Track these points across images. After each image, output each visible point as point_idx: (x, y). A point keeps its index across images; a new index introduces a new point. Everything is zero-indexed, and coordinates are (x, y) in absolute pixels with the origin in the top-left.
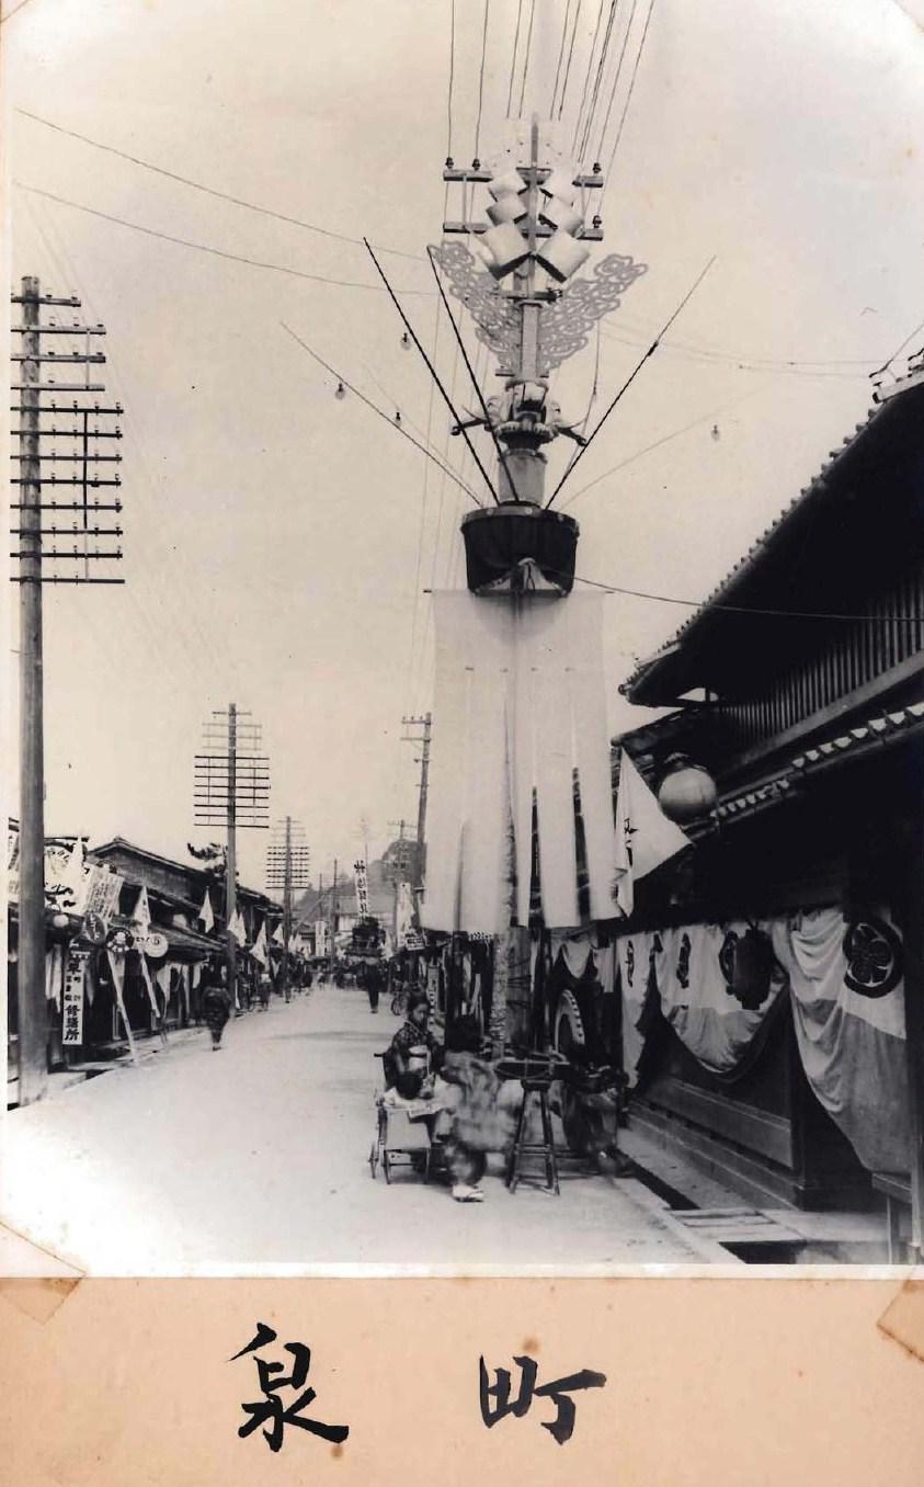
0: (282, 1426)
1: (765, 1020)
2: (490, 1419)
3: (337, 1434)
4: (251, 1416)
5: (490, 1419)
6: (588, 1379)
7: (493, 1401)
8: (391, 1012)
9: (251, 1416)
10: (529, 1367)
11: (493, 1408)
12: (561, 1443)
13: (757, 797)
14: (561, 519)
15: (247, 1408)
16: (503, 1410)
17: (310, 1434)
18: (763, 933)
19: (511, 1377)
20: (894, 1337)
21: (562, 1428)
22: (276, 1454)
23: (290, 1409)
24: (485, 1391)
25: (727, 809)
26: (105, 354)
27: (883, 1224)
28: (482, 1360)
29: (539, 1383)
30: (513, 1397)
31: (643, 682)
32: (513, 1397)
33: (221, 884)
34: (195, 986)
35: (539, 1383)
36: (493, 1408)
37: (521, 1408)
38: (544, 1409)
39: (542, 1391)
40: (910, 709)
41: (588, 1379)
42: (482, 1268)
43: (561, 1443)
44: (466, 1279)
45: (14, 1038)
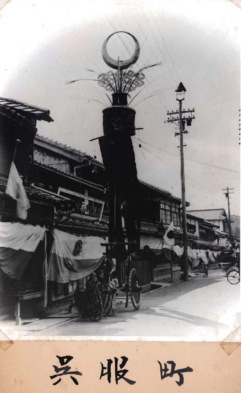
0: (103, 370)
1: (129, 274)
2: (163, 377)
3: (132, 382)
5: (163, 377)
6: (189, 369)
7: (163, 372)
11: (163, 374)
12: (114, 358)
13: (78, 248)
14: (44, 226)
16: (166, 376)
17: (126, 382)
22: (193, 372)
23: (120, 375)
24: (162, 370)
26: (176, 100)
29: (176, 369)
32: (169, 372)
33: (205, 246)
34: (88, 279)
35: (176, 369)
36: (163, 374)
37: (171, 375)
38: (176, 377)
40: (123, 227)
41: (189, 369)
43: (114, 358)
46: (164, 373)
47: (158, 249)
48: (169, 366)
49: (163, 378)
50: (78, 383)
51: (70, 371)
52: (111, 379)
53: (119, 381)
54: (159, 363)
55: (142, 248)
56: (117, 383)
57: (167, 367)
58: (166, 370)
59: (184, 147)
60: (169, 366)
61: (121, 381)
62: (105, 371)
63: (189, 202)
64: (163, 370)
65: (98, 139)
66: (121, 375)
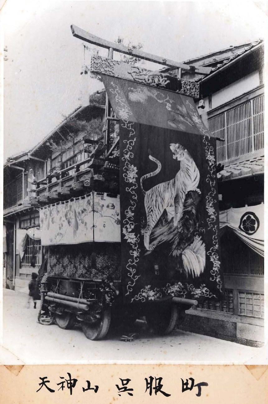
2: (184, 390)
4: (44, 385)
5: (184, 390)
6: (205, 384)
8: (37, 320)
9: (44, 385)
10: (192, 380)
15: (40, 384)
16: (187, 389)
18: (176, 143)
19: (77, 381)
20: (114, 364)
21: (199, 395)
24: (183, 384)
25: (121, 92)
27: (254, 279)
28: (71, 394)
29: (195, 384)
30: (189, 386)
31: (250, 52)
32: (189, 386)
37: (191, 389)
38: (196, 389)
39: (195, 386)
41: (205, 384)
42: (119, 362)
44: (115, 364)
45: (126, 341)
46: (185, 387)
47: (84, 165)
48: (190, 382)
49: (184, 391)
50: (76, 380)
51: (127, 389)
52: (77, 382)
53: (157, 393)
54: (182, 380)
55: (63, 274)
56: (156, 394)
57: (160, 382)
58: (187, 384)
59: (64, 388)
60: (190, 382)
61: (159, 393)
62: (149, 386)
63: (74, 37)
64: (69, 383)
65: (90, 388)
66: (159, 388)
